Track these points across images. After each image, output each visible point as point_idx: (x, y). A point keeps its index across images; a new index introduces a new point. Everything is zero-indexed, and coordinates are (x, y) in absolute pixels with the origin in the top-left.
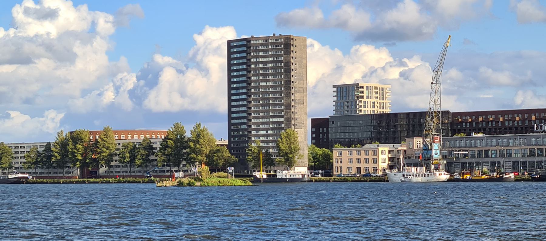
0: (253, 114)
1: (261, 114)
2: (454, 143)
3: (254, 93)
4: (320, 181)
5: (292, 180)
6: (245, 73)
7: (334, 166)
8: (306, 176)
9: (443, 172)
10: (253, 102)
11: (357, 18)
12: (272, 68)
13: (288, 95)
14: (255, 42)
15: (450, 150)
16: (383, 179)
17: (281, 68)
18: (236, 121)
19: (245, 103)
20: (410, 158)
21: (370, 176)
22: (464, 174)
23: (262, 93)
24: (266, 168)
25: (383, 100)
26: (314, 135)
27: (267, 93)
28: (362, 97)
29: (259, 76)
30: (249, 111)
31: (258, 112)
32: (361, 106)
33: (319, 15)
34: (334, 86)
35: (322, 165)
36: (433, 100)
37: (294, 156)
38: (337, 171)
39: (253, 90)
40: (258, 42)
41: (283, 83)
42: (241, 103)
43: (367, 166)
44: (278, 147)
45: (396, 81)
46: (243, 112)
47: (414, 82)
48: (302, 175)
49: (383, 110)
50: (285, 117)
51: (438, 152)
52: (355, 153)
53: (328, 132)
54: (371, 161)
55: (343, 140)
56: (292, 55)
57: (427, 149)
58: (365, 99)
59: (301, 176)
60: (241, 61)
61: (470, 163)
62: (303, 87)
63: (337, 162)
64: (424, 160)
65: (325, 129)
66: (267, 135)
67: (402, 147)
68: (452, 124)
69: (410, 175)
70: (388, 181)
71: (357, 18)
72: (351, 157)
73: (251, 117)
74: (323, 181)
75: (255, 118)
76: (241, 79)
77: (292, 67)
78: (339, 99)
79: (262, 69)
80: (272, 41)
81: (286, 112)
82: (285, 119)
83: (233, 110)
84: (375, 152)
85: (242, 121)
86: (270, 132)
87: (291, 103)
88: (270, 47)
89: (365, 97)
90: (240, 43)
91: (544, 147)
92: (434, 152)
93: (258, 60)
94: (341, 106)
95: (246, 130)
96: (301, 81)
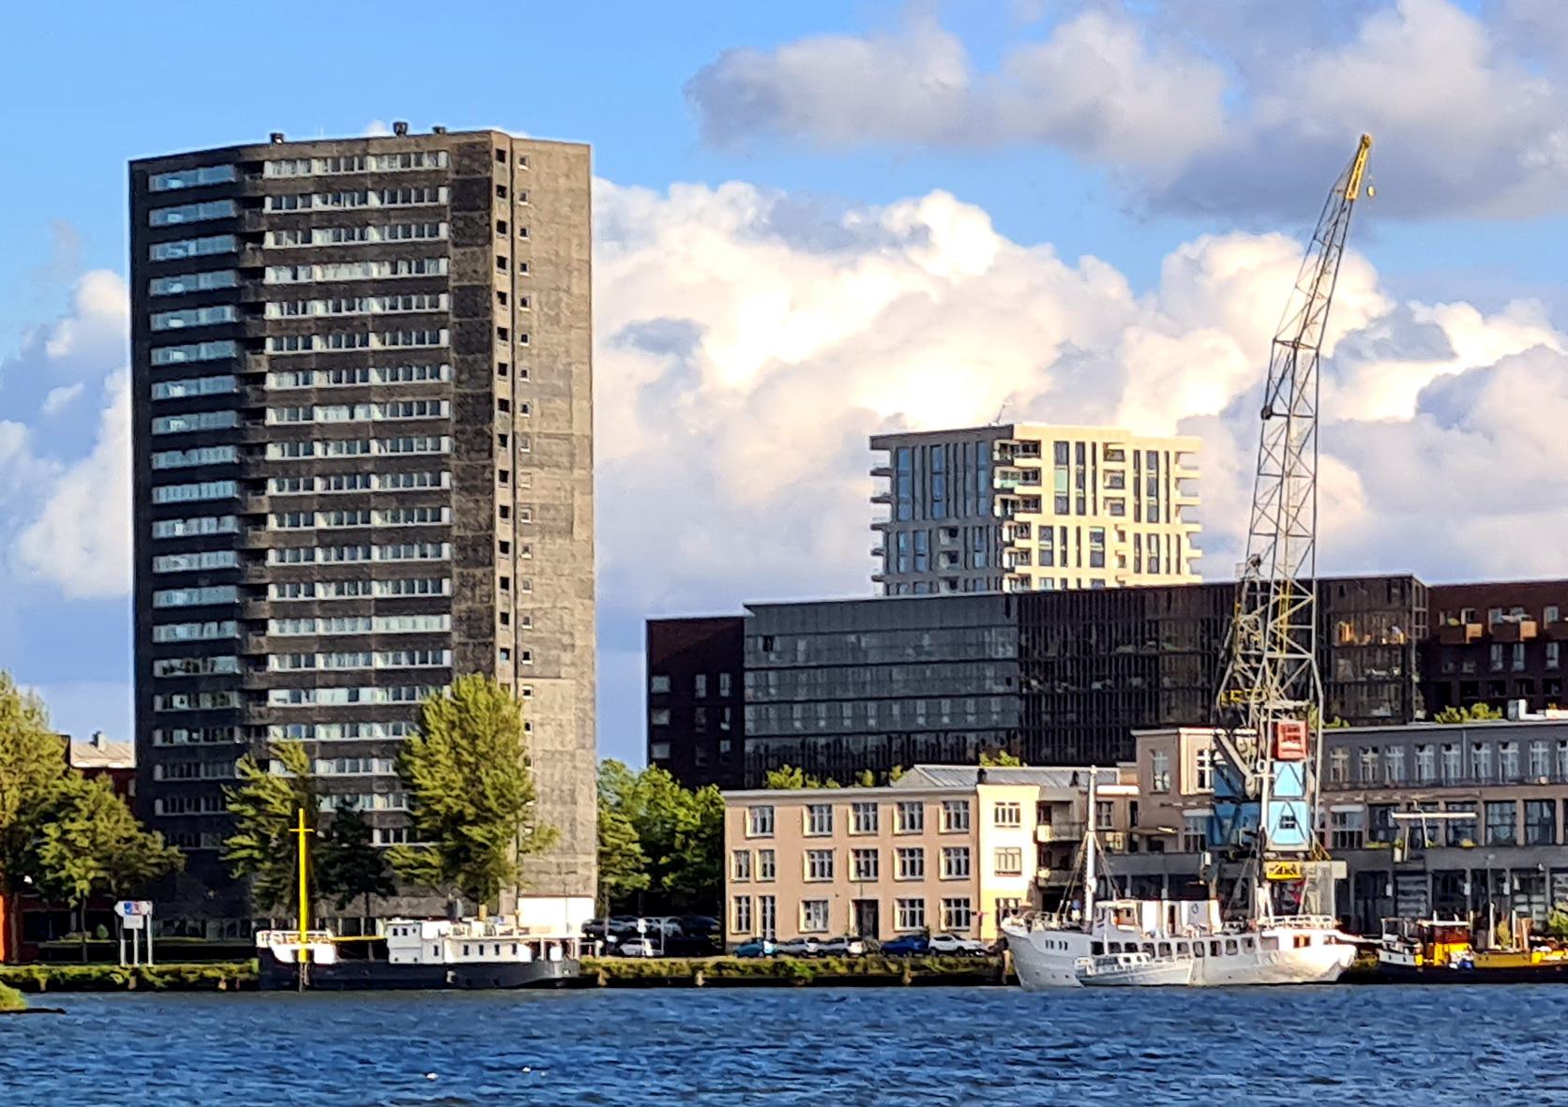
0: (273, 593)
1: (321, 592)
2: (1409, 760)
3: (282, 470)
4: (640, 980)
5: (476, 977)
6: (228, 349)
7: (732, 891)
8: (556, 953)
9: (1321, 926)
10: (272, 522)
11: (1161, 99)
12: (383, 324)
13: (477, 483)
14: (286, 171)
15: (1378, 798)
16: (988, 971)
17: (436, 321)
18: (182, 632)
19: (230, 524)
20: (1156, 845)
21: (925, 950)
22: (1429, 937)
23: (328, 470)
24: (341, 906)
25: (1153, 519)
26: (663, 719)
27: (355, 470)
28: (1034, 503)
29: (307, 373)
30: (253, 573)
31: (306, 578)
32: (1026, 553)
33: (943, 68)
34: (877, 443)
35: (671, 888)
36: (1272, 511)
37: (494, 839)
38: (744, 923)
39: (273, 453)
40: (301, 170)
41: (445, 409)
42: (207, 526)
43: (912, 892)
44: (408, 783)
45: (1230, 412)
46: (218, 577)
47: (1490, 436)
48: (535, 946)
49: (1098, 573)
50: (460, 607)
51: (1302, 811)
52: (844, 816)
53: (738, 701)
54: (936, 864)
55: (872, 741)
56: (500, 246)
57: (1234, 795)
58: (1048, 515)
59: (524, 955)
60: (206, 282)
61: (1480, 876)
62: (567, 438)
63: (744, 872)
64: (1210, 860)
65: (725, 679)
66: (353, 716)
67: (1117, 784)
68: (1431, 650)
69: (1131, 948)
70: (1013, 980)
71: (1161, 99)
72: (868, 843)
73: (261, 609)
74: (656, 981)
75: (284, 612)
76: (207, 386)
77: (501, 317)
78: (905, 512)
79: (326, 327)
80: (385, 167)
81: (464, 582)
82: (458, 621)
83: (164, 564)
84: (961, 817)
85: (211, 631)
86: (372, 696)
87: (491, 525)
88: (374, 201)
89: (1048, 504)
90: (203, 177)
91: (1559, 794)
92: (1271, 814)
93: (309, 275)
94: (917, 555)
95: (232, 681)
96: (560, 403)
